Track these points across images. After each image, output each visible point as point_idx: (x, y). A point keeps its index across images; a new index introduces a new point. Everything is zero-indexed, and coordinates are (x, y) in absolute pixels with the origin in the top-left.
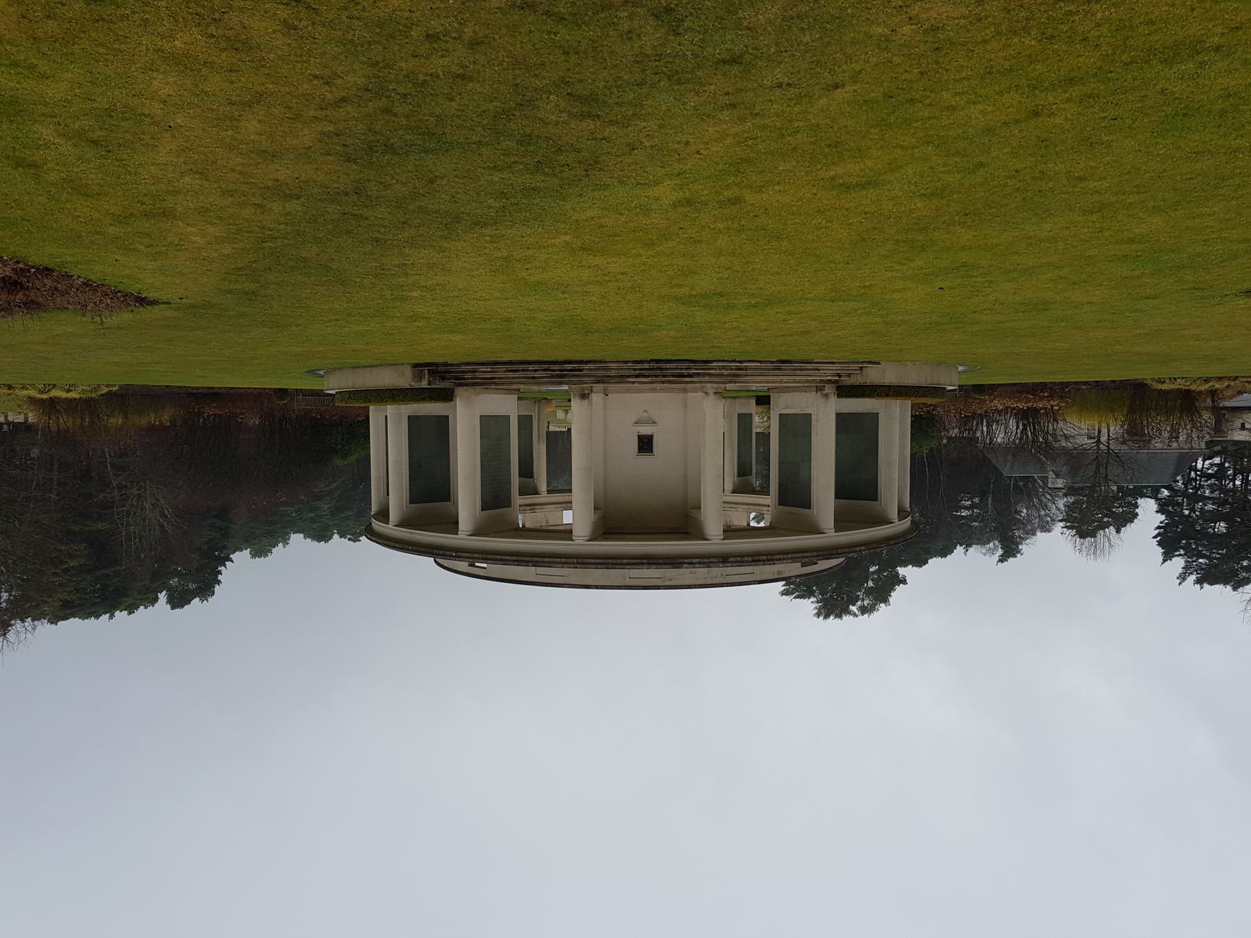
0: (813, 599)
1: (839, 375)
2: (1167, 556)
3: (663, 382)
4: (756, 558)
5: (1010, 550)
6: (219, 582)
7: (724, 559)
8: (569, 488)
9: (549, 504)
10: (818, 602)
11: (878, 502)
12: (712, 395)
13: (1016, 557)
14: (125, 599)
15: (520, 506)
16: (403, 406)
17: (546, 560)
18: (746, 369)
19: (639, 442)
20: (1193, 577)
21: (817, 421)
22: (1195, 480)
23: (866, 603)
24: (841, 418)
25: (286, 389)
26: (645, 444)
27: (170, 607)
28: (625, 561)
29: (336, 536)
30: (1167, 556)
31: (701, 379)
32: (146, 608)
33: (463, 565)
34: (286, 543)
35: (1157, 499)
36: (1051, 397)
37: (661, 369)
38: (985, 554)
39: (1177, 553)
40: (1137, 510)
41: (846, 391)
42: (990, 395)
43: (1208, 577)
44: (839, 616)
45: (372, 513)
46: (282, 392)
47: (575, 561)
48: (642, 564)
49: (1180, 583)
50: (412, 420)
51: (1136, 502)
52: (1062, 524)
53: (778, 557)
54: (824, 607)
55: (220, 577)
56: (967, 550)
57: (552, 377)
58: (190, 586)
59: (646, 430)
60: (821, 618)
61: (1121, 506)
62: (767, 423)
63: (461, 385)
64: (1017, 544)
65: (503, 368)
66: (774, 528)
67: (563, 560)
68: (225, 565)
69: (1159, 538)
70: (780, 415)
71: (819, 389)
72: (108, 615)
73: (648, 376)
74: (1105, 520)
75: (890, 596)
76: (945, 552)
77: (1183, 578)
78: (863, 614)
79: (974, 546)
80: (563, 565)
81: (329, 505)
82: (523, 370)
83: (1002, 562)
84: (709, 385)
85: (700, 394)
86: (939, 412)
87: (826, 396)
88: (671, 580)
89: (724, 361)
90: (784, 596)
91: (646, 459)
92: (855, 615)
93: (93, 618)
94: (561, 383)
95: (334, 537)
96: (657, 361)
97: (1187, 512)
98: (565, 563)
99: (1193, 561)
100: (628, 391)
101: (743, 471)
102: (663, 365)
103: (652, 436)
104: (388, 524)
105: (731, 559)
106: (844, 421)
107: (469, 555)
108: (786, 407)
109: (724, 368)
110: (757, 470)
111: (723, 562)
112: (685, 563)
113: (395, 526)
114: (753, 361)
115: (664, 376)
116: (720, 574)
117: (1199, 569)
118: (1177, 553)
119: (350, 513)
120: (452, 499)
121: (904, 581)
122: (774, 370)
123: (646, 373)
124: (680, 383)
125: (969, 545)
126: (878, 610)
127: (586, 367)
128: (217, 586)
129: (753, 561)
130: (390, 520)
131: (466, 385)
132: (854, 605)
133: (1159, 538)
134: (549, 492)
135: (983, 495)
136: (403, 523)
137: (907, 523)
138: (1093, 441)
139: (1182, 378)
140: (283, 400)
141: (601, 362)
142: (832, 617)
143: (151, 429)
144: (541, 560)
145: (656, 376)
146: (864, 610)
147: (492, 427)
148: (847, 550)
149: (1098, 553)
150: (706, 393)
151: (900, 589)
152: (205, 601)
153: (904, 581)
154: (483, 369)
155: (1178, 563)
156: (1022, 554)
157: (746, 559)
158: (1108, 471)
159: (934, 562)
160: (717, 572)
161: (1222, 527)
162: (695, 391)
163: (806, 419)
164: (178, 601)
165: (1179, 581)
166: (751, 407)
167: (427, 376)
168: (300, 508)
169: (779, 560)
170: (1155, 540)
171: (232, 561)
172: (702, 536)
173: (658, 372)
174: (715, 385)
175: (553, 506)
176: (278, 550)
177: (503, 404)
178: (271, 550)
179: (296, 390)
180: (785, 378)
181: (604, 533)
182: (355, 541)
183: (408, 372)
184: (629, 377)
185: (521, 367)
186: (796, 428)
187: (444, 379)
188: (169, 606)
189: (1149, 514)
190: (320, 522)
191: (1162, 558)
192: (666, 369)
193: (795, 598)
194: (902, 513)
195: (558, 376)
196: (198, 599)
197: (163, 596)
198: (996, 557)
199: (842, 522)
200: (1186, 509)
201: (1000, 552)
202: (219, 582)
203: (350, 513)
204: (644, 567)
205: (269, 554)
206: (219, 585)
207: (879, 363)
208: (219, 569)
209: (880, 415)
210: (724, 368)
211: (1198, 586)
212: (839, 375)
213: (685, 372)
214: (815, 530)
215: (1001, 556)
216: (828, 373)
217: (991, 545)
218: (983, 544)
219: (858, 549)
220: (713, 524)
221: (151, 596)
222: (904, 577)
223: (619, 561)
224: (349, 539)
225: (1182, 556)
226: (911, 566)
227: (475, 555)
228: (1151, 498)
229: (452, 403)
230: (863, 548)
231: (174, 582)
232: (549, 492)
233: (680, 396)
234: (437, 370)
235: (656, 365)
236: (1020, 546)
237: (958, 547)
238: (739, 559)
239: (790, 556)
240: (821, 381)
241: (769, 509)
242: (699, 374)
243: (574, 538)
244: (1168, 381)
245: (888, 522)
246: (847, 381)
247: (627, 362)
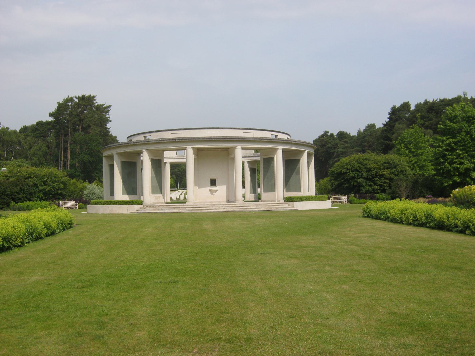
0: (96, 104)
29: (335, 134)
32: (420, 103)
44: (83, 96)
50: (299, 190)
55: (388, 116)
72: (435, 100)
91: (213, 177)
93: (448, 99)
103: (211, 185)
113: (236, 147)
120: (284, 161)
137: (106, 153)
146: (71, 100)
163: (154, 192)
164: (406, 106)
176: (363, 128)
193: (104, 105)
194: (111, 158)
197: (413, 108)
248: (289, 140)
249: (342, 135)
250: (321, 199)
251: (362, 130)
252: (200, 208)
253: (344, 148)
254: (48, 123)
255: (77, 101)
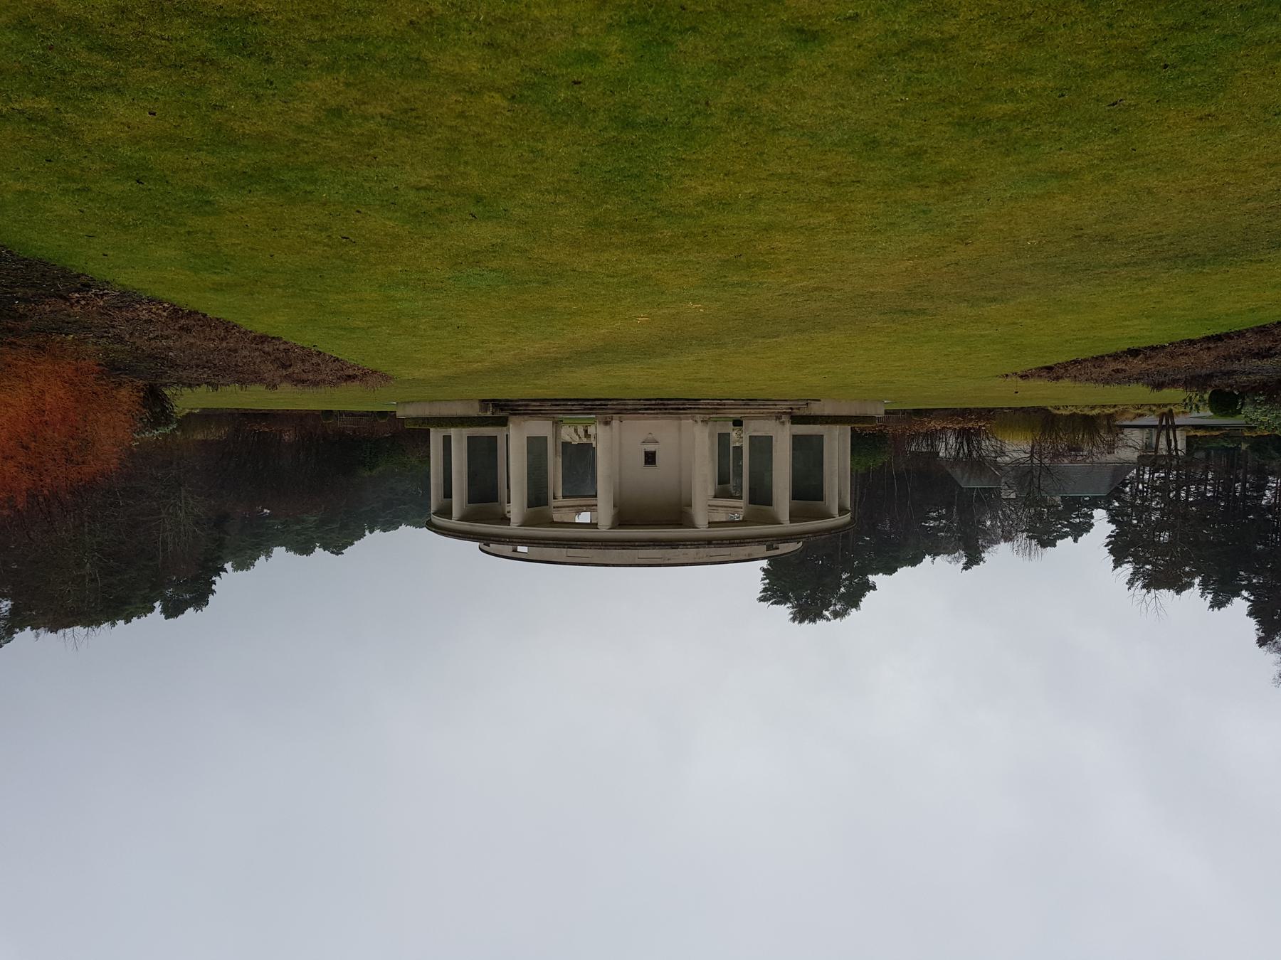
0: (789, 605)
1: (791, 409)
2: (1118, 563)
3: (665, 413)
4: (732, 541)
5: (973, 559)
6: (213, 592)
7: (709, 542)
8: (594, 494)
9: (564, 507)
10: (793, 607)
11: (824, 502)
12: (700, 423)
13: (979, 564)
14: (127, 607)
15: (554, 508)
16: (452, 429)
17: (579, 543)
18: (724, 405)
19: (645, 457)
20: (1139, 584)
21: (777, 441)
22: (1142, 492)
23: (838, 607)
24: (796, 439)
25: (332, 411)
26: (650, 458)
27: (164, 616)
28: (637, 544)
30: (1118, 563)
31: (692, 411)
33: (507, 549)
34: (268, 555)
35: (1108, 510)
36: (979, 419)
37: (664, 405)
38: (950, 562)
39: (1126, 560)
40: (1093, 521)
41: (796, 420)
42: (928, 417)
43: (1153, 583)
44: (813, 620)
45: (432, 512)
46: (329, 413)
47: (600, 543)
48: (649, 545)
49: (1129, 588)
51: (1092, 513)
52: (1025, 535)
53: (748, 540)
54: (799, 612)
56: (934, 559)
57: (585, 409)
58: (185, 596)
59: (651, 448)
60: (797, 622)
61: (1078, 517)
62: (741, 439)
63: (515, 414)
64: (980, 553)
65: (549, 403)
66: (746, 521)
67: (591, 543)
68: (219, 575)
69: (1110, 547)
70: (750, 436)
71: (778, 418)
73: (654, 409)
74: (1065, 530)
75: (861, 601)
76: (915, 561)
77: (1131, 583)
78: (835, 618)
79: (942, 555)
80: (591, 547)
81: (316, 518)
82: (564, 405)
83: (966, 569)
84: (698, 416)
85: (691, 421)
86: (888, 431)
87: (783, 423)
88: (669, 559)
89: (708, 399)
90: (762, 603)
91: (650, 469)
92: (828, 619)
94: (591, 414)
95: (315, 550)
96: (661, 399)
97: (1135, 522)
98: (592, 545)
99: (1140, 568)
100: (639, 419)
101: (723, 479)
102: (666, 402)
103: (655, 452)
104: (451, 519)
105: (714, 542)
106: (797, 441)
107: (520, 540)
108: (755, 431)
109: (708, 404)
110: (733, 467)
111: (708, 544)
112: (680, 545)
113: (458, 520)
114: (729, 399)
115: (666, 409)
116: (705, 556)
117: (1146, 574)
118: (1126, 560)
119: (334, 526)
121: (874, 588)
122: (744, 405)
123: (653, 407)
124: (677, 414)
125: (937, 554)
126: (849, 614)
127: (610, 403)
128: (211, 596)
129: (730, 543)
130: (453, 516)
131: (519, 414)
132: (828, 610)
133: (1110, 547)
134: (564, 497)
135: (949, 507)
136: (463, 518)
137: (847, 518)
138: (1028, 455)
139: (1073, 406)
140: (329, 420)
141: (621, 400)
142: (806, 622)
143: (204, 443)
144: (575, 543)
145: (660, 409)
146: (836, 615)
147: (536, 447)
148: (799, 536)
149: (1033, 553)
150: (696, 421)
151: (870, 595)
152: (200, 611)
153: (874, 588)
154: (534, 403)
155: (1127, 569)
156: (984, 562)
157: (725, 542)
158: (1041, 482)
159: (904, 572)
160: (703, 552)
161: (1165, 536)
162: (687, 419)
164: (172, 611)
165: (1128, 586)
166: (729, 428)
167: (491, 408)
168: (287, 521)
169: (749, 542)
170: (1107, 548)
171: (227, 572)
172: (692, 525)
173: (662, 407)
174: (702, 416)
175: (567, 509)
177: (540, 427)
178: (253, 563)
179: (339, 411)
180: (752, 411)
181: (619, 525)
182: (337, 554)
183: (477, 405)
184: (640, 410)
185: (562, 403)
186: (762, 446)
187: (502, 410)
188: (163, 616)
189: (1102, 527)
190: (304, 534)
191: (1113, 565)
192: (668, 404)
193: (772, 604)
194: (842, 511)
195: (590, 409)
196: (192, 609)
198: (961, 565)
199: (794, 517)
200: (1135, 519)
201: (964, 560)
202: (213, 592)
203: (334, 526)
204: (650, 547)
205: (252, 567)
206: (213, 594)
207: (819, 400)
208: (214, 578)
209: (824, 437)
210: (708, 404)
211: (1145, 591)
212: (791, 409)
213: (681, 407)
214: (775, 521)
215: (966, 564)
216: (783, 407)
217: (957, 554)
218: (949, 554)
219: (807, 536)
220: (701, 516)
221: (148, 605)
222: (874, 583)
223: (632, 544)
224: (332, 552)
225: (1131, 562)
226: (881, 574)
227: (525, 541)
228: (1103, 509)
229: (505, 428)
230: (810, 535)
231: (169, 592)
232: (564, 497)
233: (676, 422)
234: (499, 404)
235: (661, 402)
236: (983, 555)
237: (927, 556)
238: (719, 542)
239: (757, 540)
240: (779, 413)
241: (741, 510)
242: (691, 408)
243: (599, 527)
244: (1062, 408)
245: (833, 517)
246: (797, 412)
247: (640, 400)
248: (485, 542)
249: (305, 549)
250: (416, 420)
251: (262, 558)
252: (646, 407)
253: (303, 521)
254: (875, 572)
255: (826, 613)
